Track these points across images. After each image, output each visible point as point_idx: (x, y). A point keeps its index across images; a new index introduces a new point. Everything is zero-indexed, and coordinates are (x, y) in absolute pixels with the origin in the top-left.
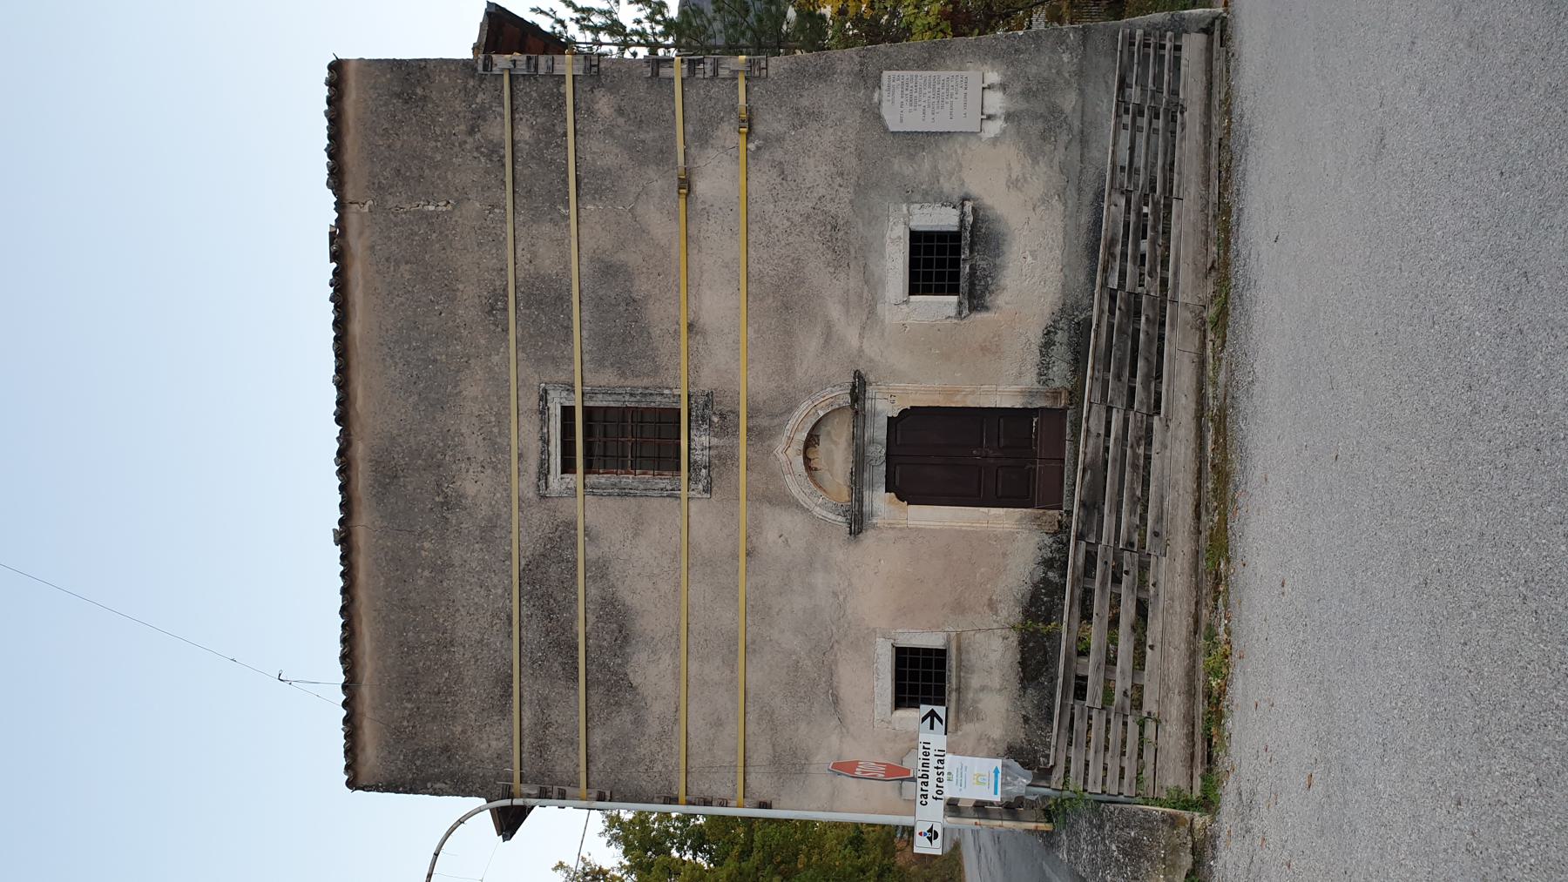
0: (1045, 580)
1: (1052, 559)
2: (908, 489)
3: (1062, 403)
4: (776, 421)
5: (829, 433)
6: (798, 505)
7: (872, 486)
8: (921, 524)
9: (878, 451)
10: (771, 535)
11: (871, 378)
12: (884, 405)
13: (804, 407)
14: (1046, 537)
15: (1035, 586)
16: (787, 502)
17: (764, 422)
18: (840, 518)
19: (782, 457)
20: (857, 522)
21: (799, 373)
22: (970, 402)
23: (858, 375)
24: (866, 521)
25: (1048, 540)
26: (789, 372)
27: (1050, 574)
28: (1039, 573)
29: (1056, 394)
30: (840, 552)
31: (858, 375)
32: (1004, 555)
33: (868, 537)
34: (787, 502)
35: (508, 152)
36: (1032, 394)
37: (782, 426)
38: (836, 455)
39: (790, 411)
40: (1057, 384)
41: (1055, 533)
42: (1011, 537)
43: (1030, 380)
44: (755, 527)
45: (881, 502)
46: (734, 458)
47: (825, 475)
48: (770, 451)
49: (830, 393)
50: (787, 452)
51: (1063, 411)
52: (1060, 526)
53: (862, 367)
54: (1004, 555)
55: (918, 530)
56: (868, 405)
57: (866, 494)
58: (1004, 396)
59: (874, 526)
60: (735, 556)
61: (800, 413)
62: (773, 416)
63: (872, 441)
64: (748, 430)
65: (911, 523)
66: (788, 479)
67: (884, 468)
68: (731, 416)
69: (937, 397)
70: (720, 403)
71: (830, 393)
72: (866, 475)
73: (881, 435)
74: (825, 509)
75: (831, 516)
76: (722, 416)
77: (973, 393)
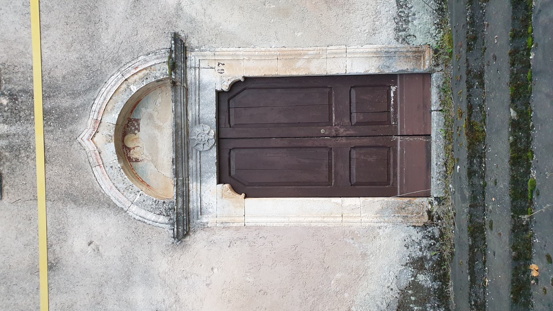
0: (415, 285)
1: (422, 259)
2: (243, 177)
3: (426, 65)
4: (79, 101)
5: (151, 117)
6: (110, 204)
7: (200, 177)
8: (261, 221)
9: (205, 132)
10: (77, 243)
11: (193, 42)
12: (211, 76)
13: (113, 82)
14: (414, 231)
15: (403, 292)
16: (93, 199)
17: (65, 102)
18: (162, 219)
19: (89, 146)
20: (183, 222)
21: (106, 39)
22: (357, 199)
23: (176, 37)
24: (195, 222)
25: (417, 235)
26: (92, 39)
27: (421, 277)
28: (407, 277)
29: (418, 54)
30: (163, 260)
31: (176, 37)
32: (364, 256)
33: (197, 241)
34: (93, 199)
35: (354, 109)
36: (389, 55)
37: (86, 107)
38: (156, 141)
39: (94, 86)
40: (420, 40)
41: (425, 226)
42: (371, 233)
43: (386, 37)
44: (57, 234)
45: (212, 196)
46: (29, 147)
47: (147, 167)
48: (73, 137)
49: (143, 62)
50: (95, 139)
51: (427, 76)
52: (431, 217)
53: (182, 28)
54: (364, 256)
55: (258, 228)
56: (191, 75)
57: (193, 186)
58: (355, 59)
59: (204, 227)
60: (34, 271)
61: (106, 91)
62: (74, 94)
63: (198, 121)
64: (46, 113)
65: (250, 221)
66: (98, 171)
67: (214, 153)
68: (24, 97)
69: (274, 63)
70: (9, 81)
71: (143, 62)
72: (192, 163)
73: (209, 112)
74: (142, 206)
75: (151, 216)
76: (13, 97)
77: (317, 56)
